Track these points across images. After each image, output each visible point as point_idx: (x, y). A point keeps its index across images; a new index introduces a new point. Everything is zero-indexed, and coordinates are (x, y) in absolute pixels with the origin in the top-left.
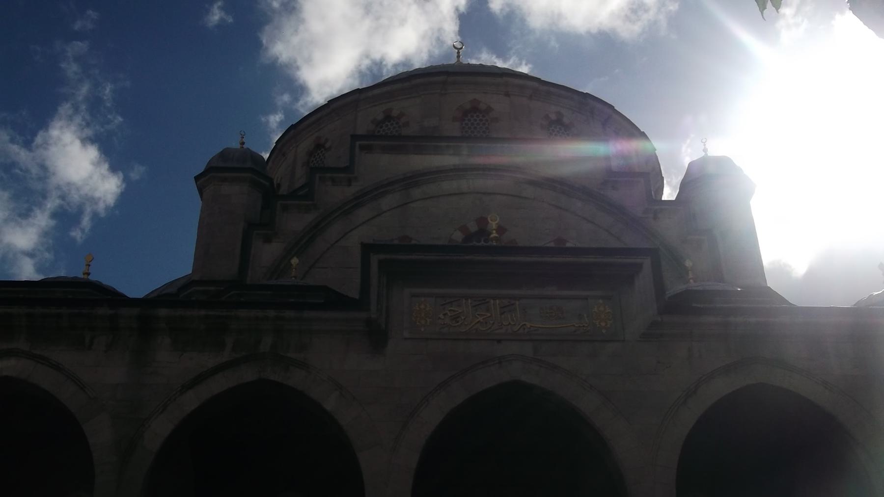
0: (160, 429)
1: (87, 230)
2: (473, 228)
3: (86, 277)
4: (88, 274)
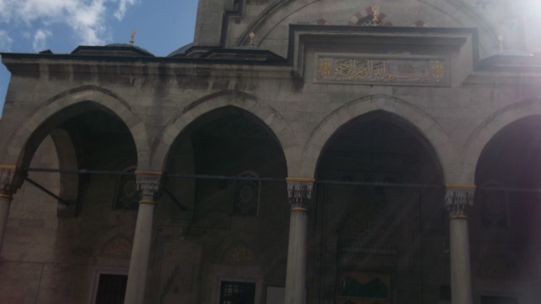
0: (172, 133)
1: (123, 13)
2: (364, 14)
3: (131, 44)
4: (133, 42)
